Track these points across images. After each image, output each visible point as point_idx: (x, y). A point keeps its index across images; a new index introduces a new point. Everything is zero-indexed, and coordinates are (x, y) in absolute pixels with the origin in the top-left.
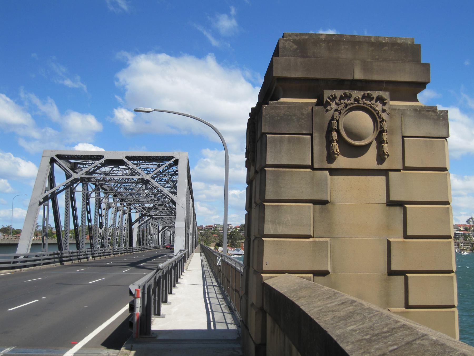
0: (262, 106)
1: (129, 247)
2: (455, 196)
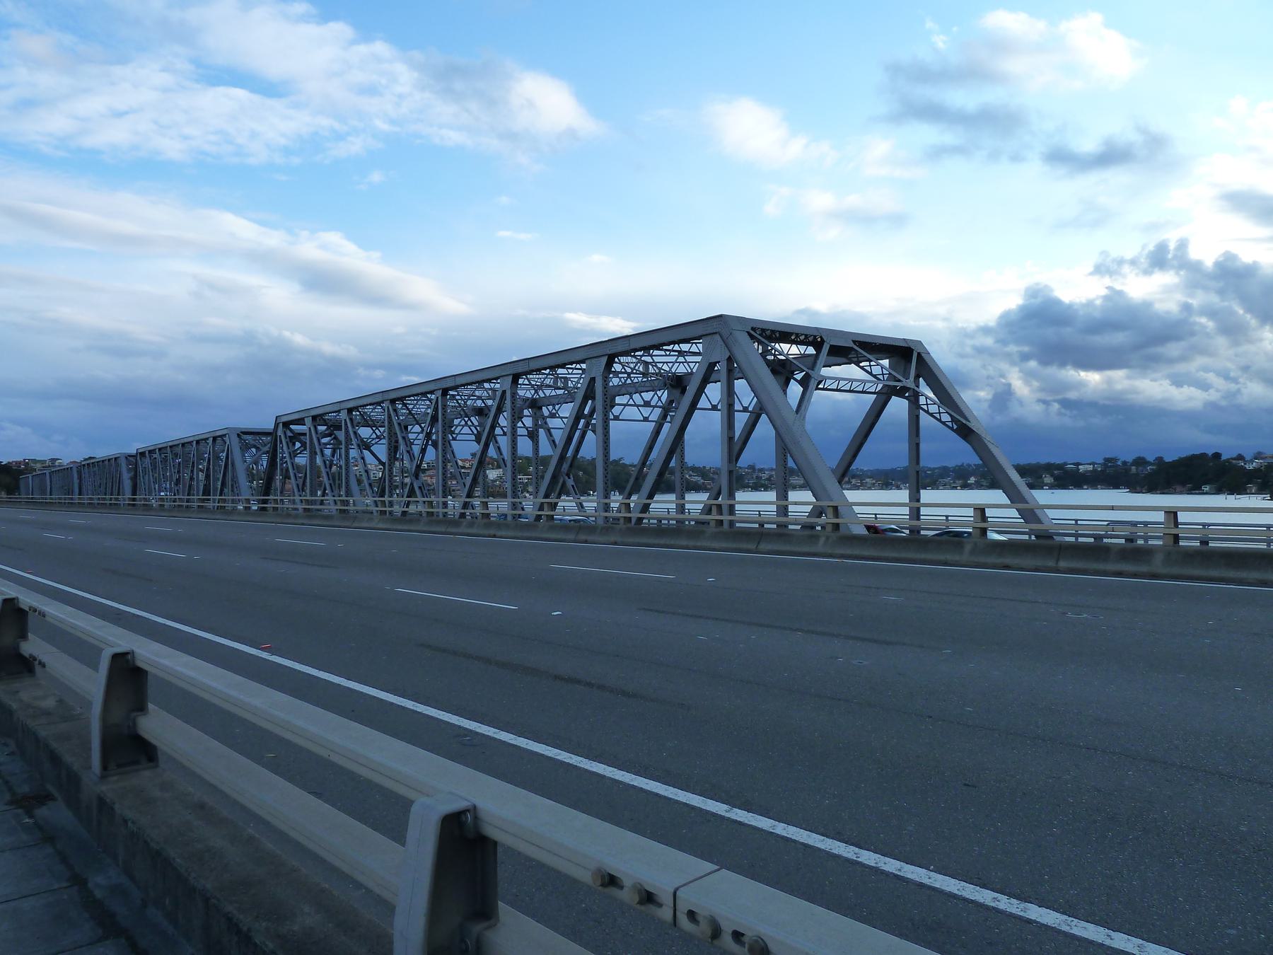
2: (796, 503)
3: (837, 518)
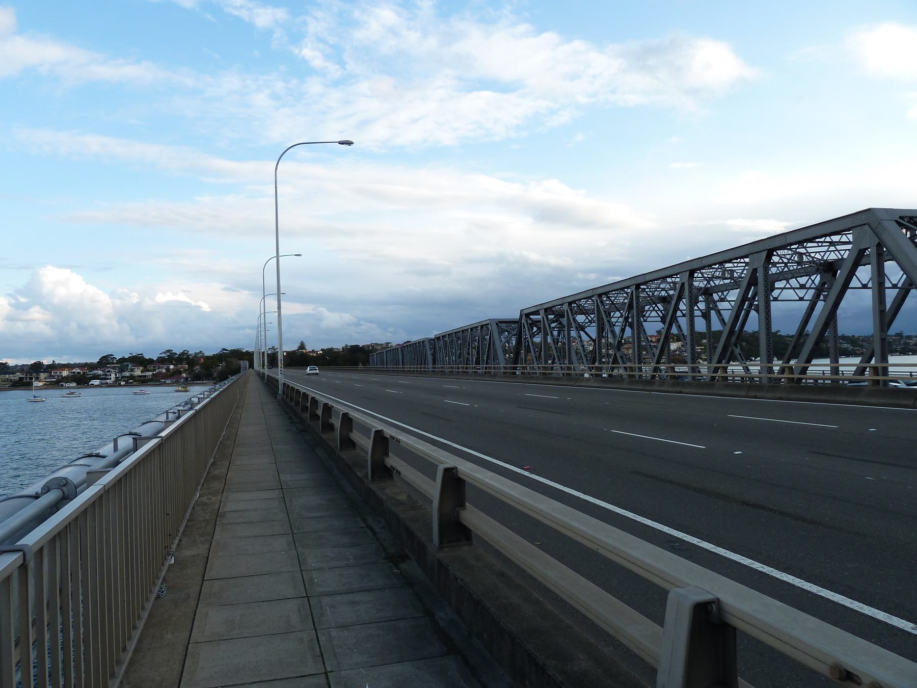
3: (883, 367)
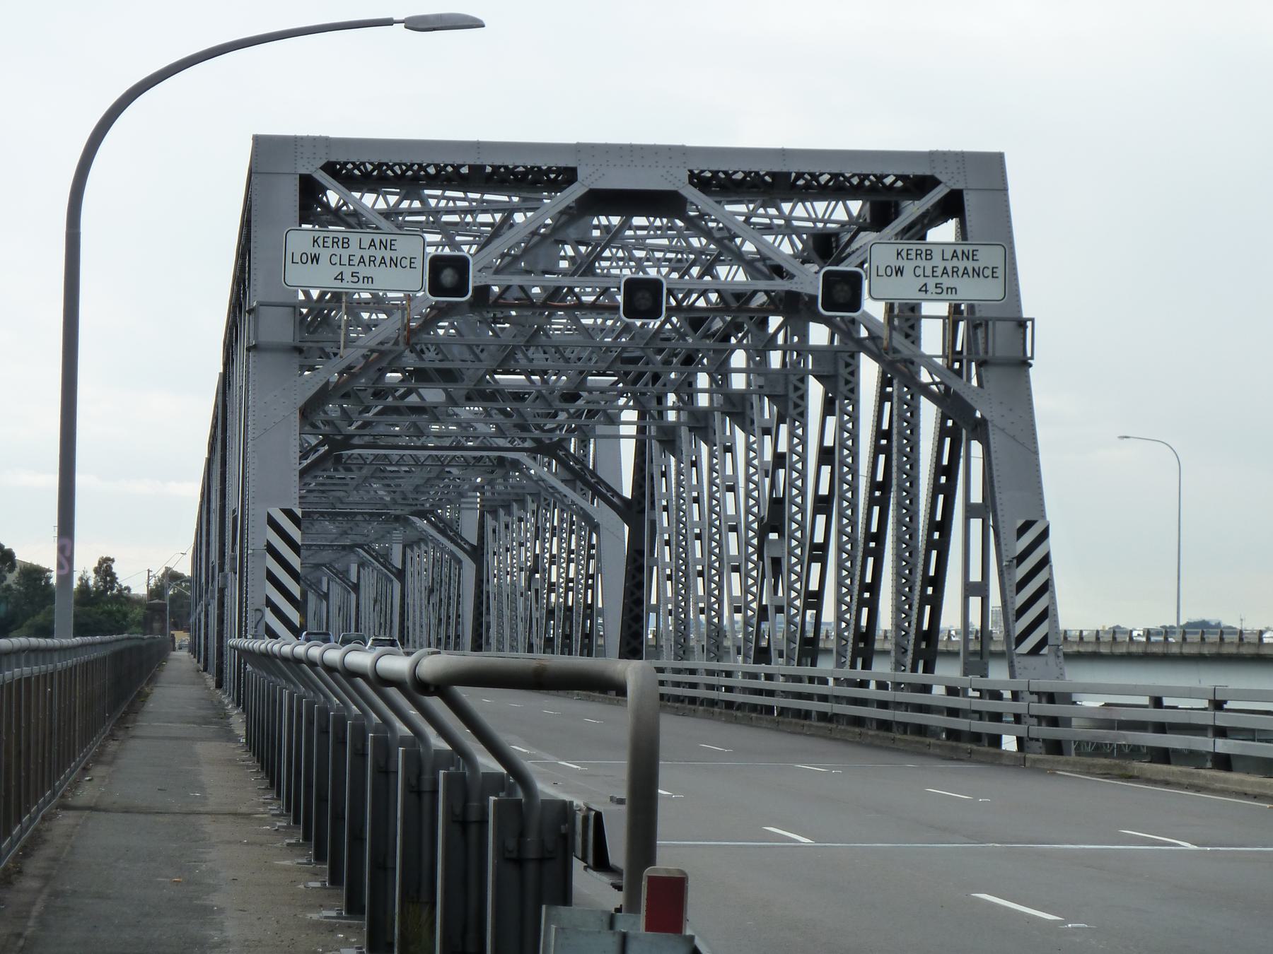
0: (925, 607)
1: (326, 865)
